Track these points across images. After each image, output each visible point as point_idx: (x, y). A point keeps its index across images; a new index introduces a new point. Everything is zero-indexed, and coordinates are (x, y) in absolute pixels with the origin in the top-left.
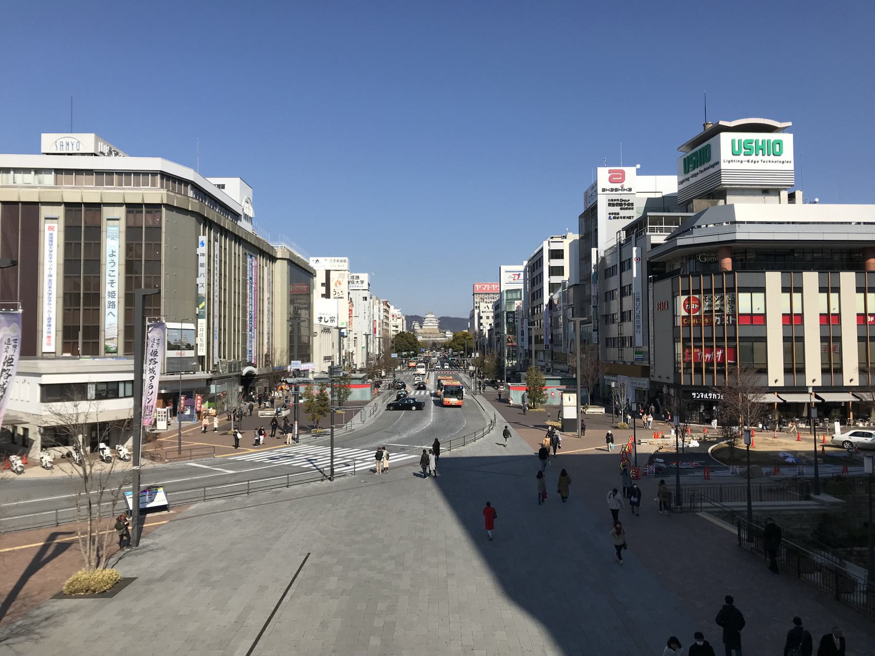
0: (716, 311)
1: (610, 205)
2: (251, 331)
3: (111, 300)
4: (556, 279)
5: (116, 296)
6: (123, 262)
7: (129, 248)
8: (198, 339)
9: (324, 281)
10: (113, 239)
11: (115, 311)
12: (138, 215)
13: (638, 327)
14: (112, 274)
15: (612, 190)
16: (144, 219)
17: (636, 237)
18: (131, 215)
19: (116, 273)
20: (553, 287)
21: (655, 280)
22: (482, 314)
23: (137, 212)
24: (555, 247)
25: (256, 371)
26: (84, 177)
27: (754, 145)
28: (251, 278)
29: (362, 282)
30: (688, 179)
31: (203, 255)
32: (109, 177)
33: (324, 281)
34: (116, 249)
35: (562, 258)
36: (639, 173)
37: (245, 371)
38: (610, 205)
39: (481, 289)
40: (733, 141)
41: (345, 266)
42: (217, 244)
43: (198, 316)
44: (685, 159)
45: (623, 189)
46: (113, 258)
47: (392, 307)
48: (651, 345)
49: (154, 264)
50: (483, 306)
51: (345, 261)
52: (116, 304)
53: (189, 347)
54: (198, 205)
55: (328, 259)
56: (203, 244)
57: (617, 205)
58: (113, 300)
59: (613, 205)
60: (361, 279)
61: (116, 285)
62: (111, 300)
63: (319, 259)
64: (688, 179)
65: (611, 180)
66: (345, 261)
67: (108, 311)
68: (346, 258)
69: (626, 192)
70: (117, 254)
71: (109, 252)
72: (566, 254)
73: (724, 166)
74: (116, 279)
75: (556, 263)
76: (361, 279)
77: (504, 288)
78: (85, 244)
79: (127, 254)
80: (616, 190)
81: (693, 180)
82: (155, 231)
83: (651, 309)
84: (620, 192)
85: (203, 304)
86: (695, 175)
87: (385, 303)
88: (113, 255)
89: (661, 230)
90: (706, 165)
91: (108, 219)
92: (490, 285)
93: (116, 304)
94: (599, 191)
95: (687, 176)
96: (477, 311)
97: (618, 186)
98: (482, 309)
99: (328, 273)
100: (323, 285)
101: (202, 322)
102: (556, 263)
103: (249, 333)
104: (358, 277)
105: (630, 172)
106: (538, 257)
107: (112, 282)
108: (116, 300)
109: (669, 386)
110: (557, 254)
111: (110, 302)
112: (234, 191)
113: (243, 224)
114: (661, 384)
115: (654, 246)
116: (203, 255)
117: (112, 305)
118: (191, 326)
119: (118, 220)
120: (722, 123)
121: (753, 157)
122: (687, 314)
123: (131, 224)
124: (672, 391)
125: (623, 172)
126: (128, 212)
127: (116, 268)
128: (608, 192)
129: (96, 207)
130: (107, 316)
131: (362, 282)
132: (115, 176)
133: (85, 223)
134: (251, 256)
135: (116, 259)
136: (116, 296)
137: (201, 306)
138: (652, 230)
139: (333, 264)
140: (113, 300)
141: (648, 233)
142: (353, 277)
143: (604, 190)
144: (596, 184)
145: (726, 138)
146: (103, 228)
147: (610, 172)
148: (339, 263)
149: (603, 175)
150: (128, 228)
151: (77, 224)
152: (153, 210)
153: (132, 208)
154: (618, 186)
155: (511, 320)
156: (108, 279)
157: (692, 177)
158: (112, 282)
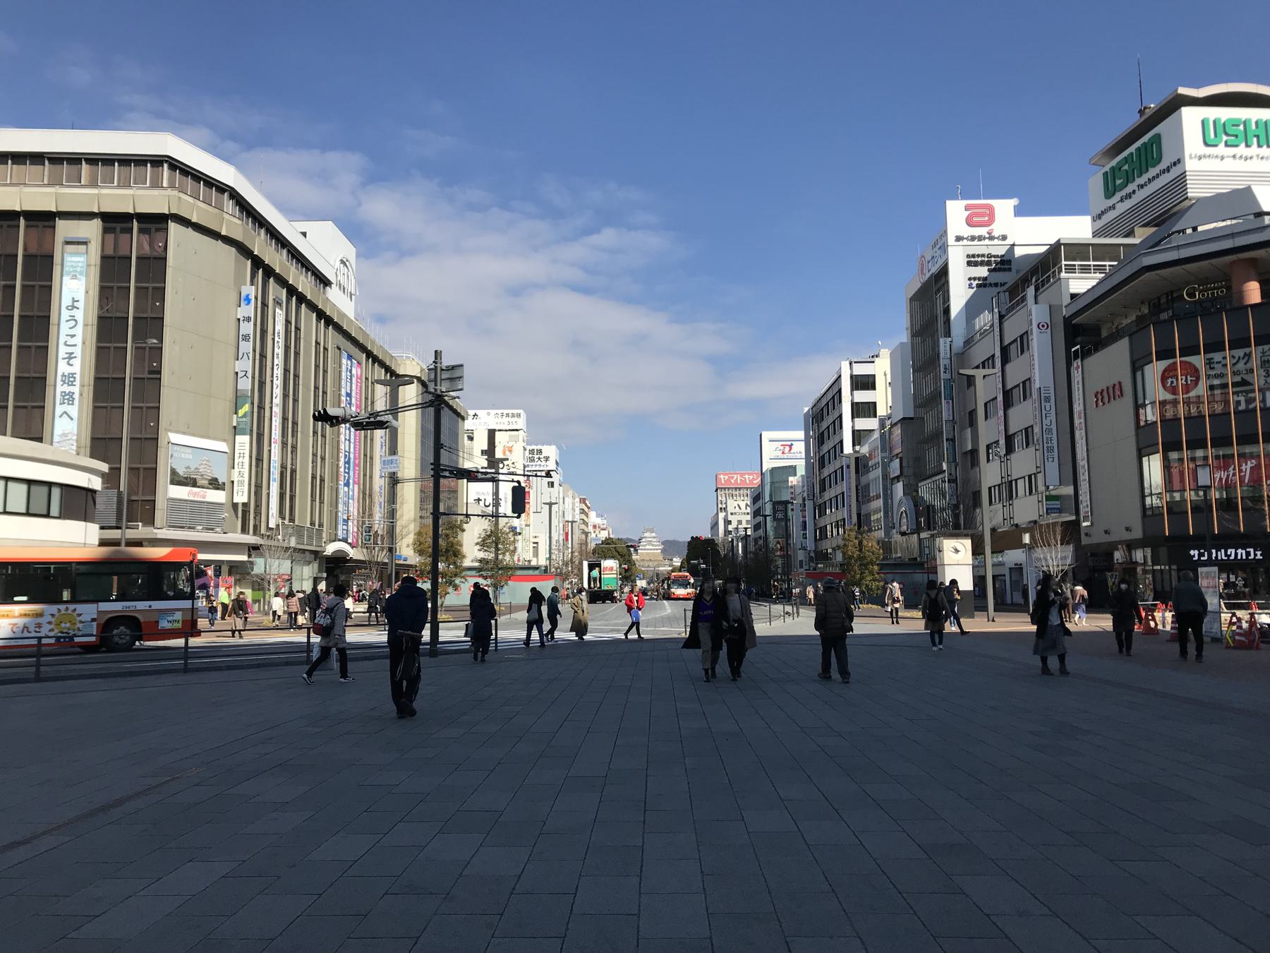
0: (1234, 385)
1: (969, 264)
2: (347, 484)
3: (67, 389)
4: (864, 424)
5: (77, 383)
6: (93, 319)
7: (106, 293)
8: (235, 473)
9: (486, 448)
10: (74, 277)
11: (74, 410)
12: (124, 238)
13: (1050, 450)
14: (71, 341)
15: (973, 238)
16: (136, 244)
17: (1036, 290)
18: (110, 237)
19: (78, 340)
20: (858, 436)
21: (1085, 354)
22: (730, 518)
23: (124, 231)
24: (860, 370)
25: (353, 553)
26: (30, 169)
27: (1241, 127)
28: (349, 395)
29: (547, 459)
30: (1113, 207)
31: (249, 319)
32: (74, 168)
33: (486, 448)
34: (81, 296)
35: (874, 388)
36: (1019, 212)
37: (331, 549)
38: (969, 264)
39: (728, 481)
40: (1204, 123)
41: (521, 423)
42: (280, 314)
43: (236, 431)
44: (1106, 174)
45: (991, 238)
46: (74, 312)
47: (592, 514)
48: (1083, 477)
49: (152, 324)
50: (732, 505)
51: (519, 415)
52: (76, 396)
53: (215, 484)
54: (241, 229)
55: (493, 412)
56: (248, 300)
57: (982, 264)
58: (71, 389)
59: (976, 264)
60: (544, 454)
61: (77, 363)
62: (67, 389)
63: (478, 412)
64: (1113, 207)
65: (970, 222)
66: (519, 415)
67: (59, 409)
68: (521, 411)
69: (996, 242)
70: (81, 305)
71: (66, 301)
72: (880, 382)
73: (1190, 165)
74: (78, 351)
75: (863, 396)
76: (544, 454)
77: (767, 466)
78: (23, 286)
79: (101, 307)
80: (980, 238)
81: (1122, 207)
82: (155, 266)
83: (1078, 407)
84: (987, 242)
85: (246, 408)
86: (1129, 196)
87: (583, 501)
88: (74, 307)
89: (1085, 269)
90: (1153, 172)
91: (68, 243)
92: (742, 475)
93: (76, 396)
94: (951, 240)
95: (1111, 202)
96: (722, 515)
97: (982, 231)
98: (730, 510)
99: (492, 434)
100: (483, 452)
101: (243, 441)
102: (863, 396)
103: (343, 490)
104: (540, 452)
105: (1004, 208)
106: (835, 389)
107: (70, 356)
108: (76, 389)
109: (1131, 546)
110: (865, 383)
111: (64, 394)
112: (324, 244)
113: (333, 294)
114: (1111, 548)
115: (1073, 296)
116: (249, 319)
117: (68, 398)
118: (223, 446)
119: (85, 243)
120: (1182, 91)
121: (1241, 150)
122: (1169, 397)
123: (110, 252)
124: (1139, 555)
125: (991, 208)
126: (106, 231)
127: (79, 331)
128: (965, 242)
129: (44, 220)
130: (58, 421)
131: (547, 459)
132: (85, 167)
133: (25, 249)
134: (350, 357)
135: (79, 315)
136: (77, 383)
137: (241, 412)
138: (1071, 269)
139: (500, 420)
140: (71, 389)
141: (1063, 275)
142: (532, 452)
143: (959, 239)
144: (946, 232)
145: (1191, 117)
146: (57, 259)
147: (967, 208)
148: (510, 419)
149: (956, 211)
150: (105, 259)
151: (9, 251)
152: (153, 227)
153: (114, 222)
154: (982, 231)
155: (780, 516)
156: (63, 351)
157: (1122, 200)
158: (70, 356)
